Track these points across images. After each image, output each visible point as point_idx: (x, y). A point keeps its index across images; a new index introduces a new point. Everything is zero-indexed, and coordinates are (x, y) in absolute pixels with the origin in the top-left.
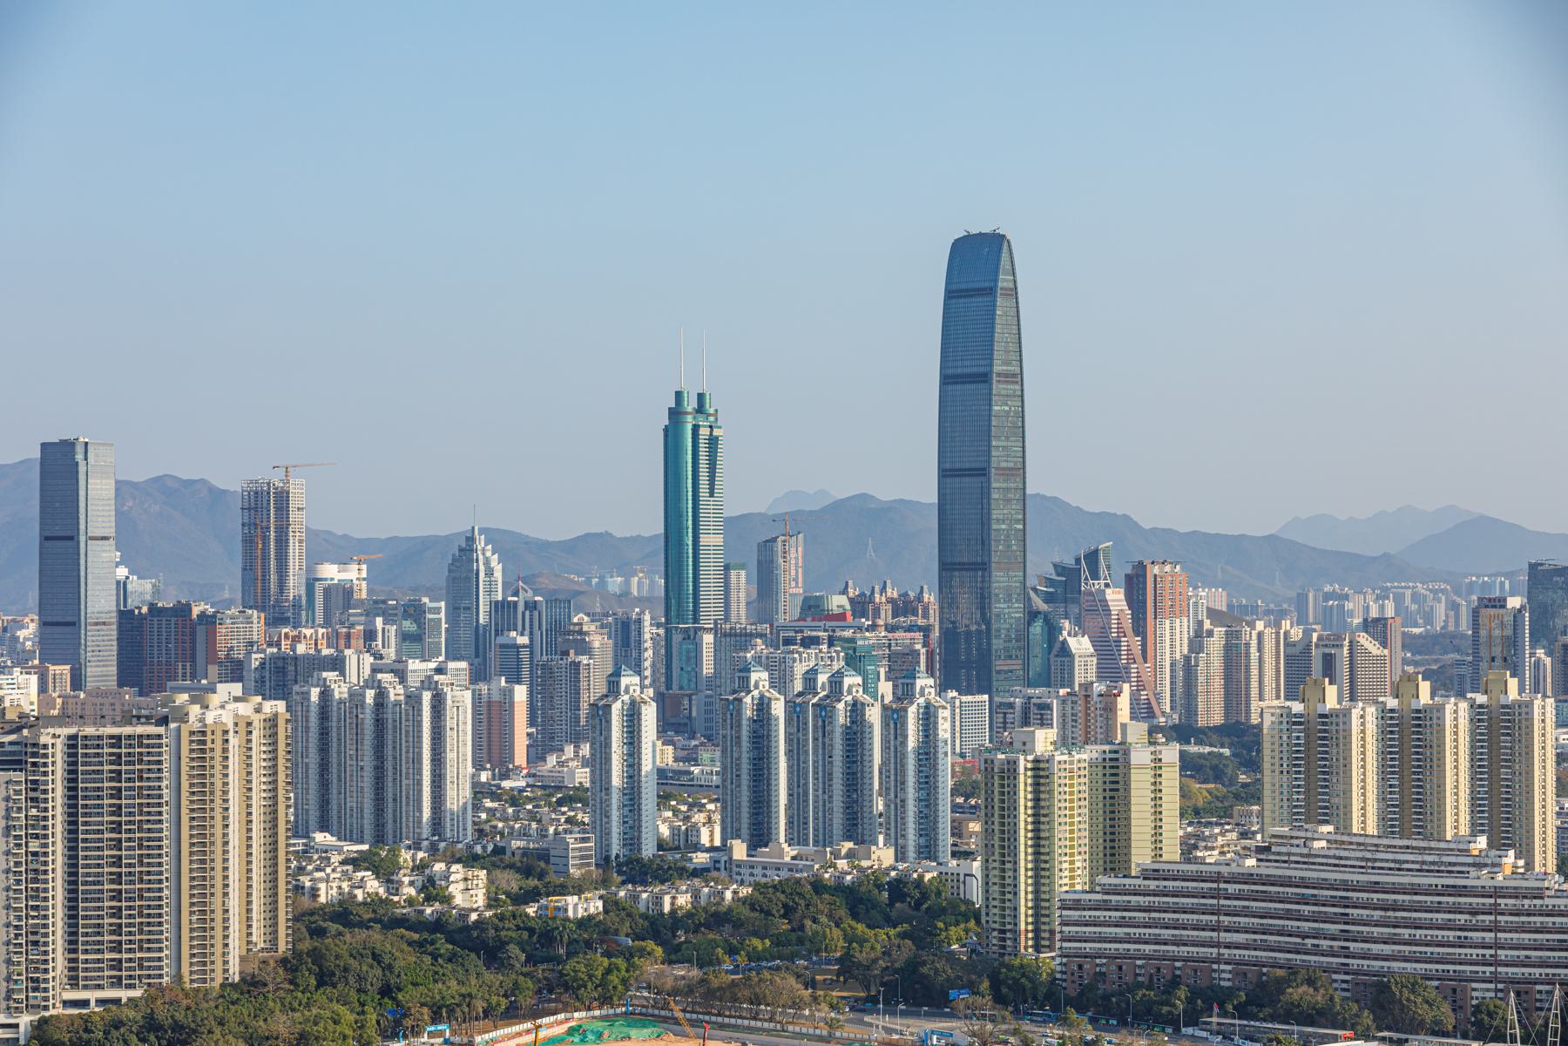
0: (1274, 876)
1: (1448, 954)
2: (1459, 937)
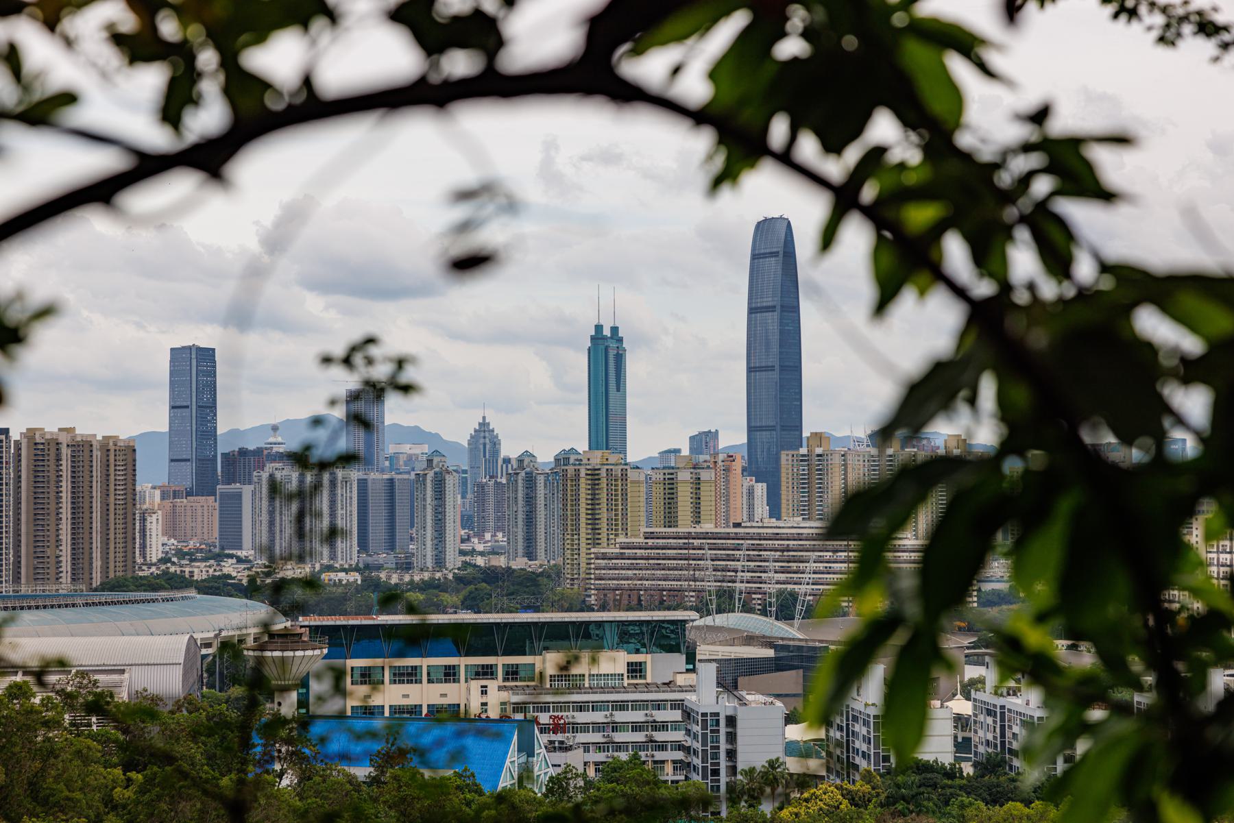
0: (720, 533)
1: (820, 578)
2: (826, 567)
